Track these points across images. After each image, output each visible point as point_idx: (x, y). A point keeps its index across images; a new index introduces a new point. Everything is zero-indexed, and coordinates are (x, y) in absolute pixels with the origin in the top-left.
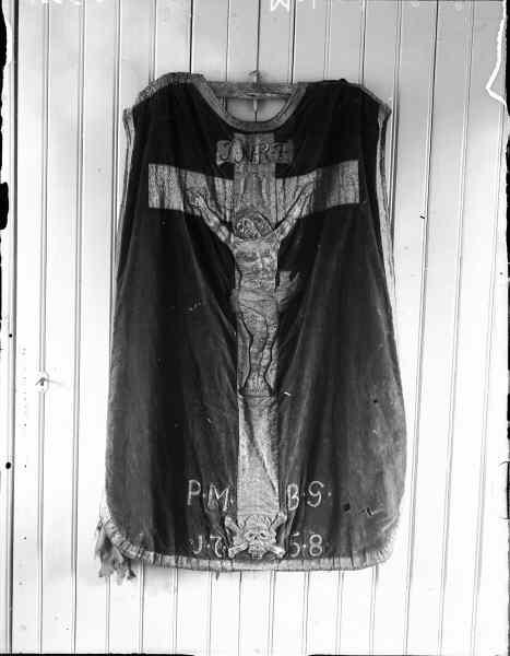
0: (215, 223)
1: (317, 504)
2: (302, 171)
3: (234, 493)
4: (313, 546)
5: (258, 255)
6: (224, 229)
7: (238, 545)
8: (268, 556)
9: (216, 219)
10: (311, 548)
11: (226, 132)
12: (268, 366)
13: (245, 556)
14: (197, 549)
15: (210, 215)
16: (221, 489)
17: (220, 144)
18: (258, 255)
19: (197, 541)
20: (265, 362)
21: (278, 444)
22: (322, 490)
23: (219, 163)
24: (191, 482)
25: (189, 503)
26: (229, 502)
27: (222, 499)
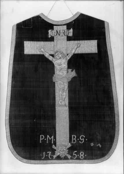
0: (48, 55)
1: (82, 143)
2: (73, 70)
3: (55, 138)
4: (83, 155)
5: (61, 66)
6: (51, 57)
7: (57, 154)
8: (66, 158)
9: (48, 54)
10: (83, 155)
11: (51, 26)
12: (65, 98)
13: (59, 158)
14: (43, 157)
15: (46, 53)
16: (51, 137)
17: (50, 31)
18: (61, 66)
19: (43, 154)
20: (64, 97)
21: (68, 73)
22: (84, 138)
23: (50, 36)
24: (41, 136)
25: (40, 142)
26: (53, 140)
27: (52, 139)
